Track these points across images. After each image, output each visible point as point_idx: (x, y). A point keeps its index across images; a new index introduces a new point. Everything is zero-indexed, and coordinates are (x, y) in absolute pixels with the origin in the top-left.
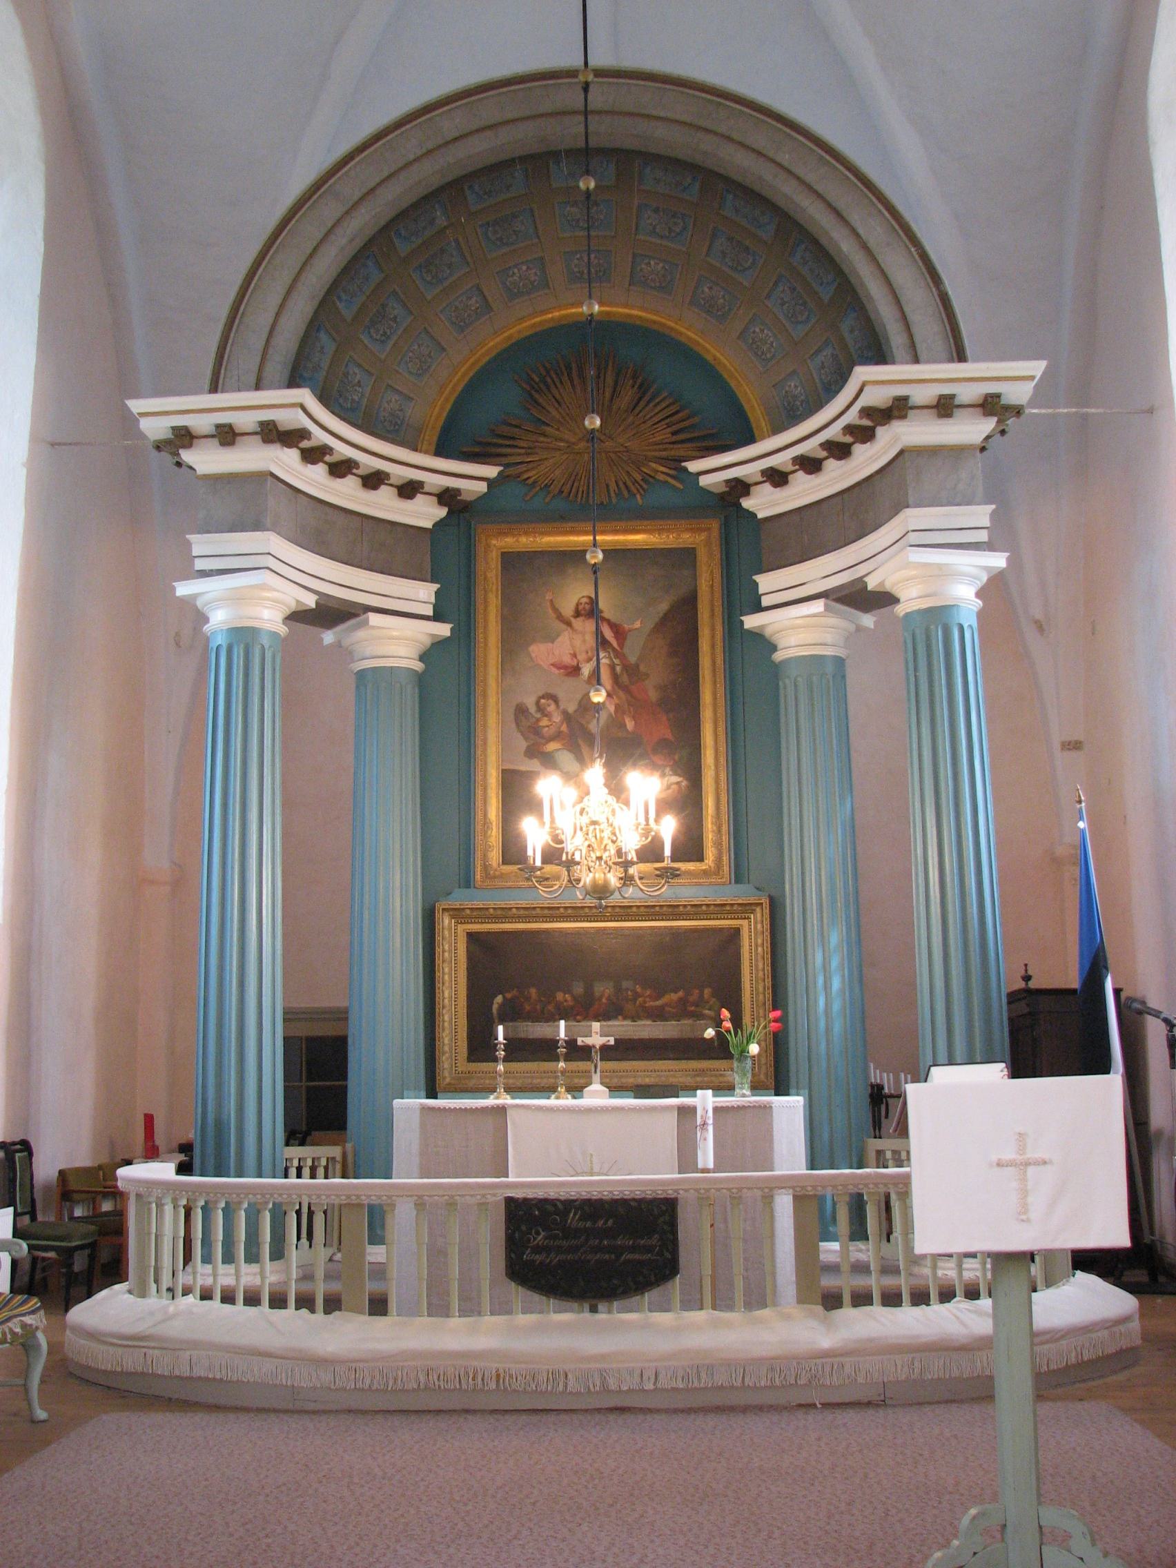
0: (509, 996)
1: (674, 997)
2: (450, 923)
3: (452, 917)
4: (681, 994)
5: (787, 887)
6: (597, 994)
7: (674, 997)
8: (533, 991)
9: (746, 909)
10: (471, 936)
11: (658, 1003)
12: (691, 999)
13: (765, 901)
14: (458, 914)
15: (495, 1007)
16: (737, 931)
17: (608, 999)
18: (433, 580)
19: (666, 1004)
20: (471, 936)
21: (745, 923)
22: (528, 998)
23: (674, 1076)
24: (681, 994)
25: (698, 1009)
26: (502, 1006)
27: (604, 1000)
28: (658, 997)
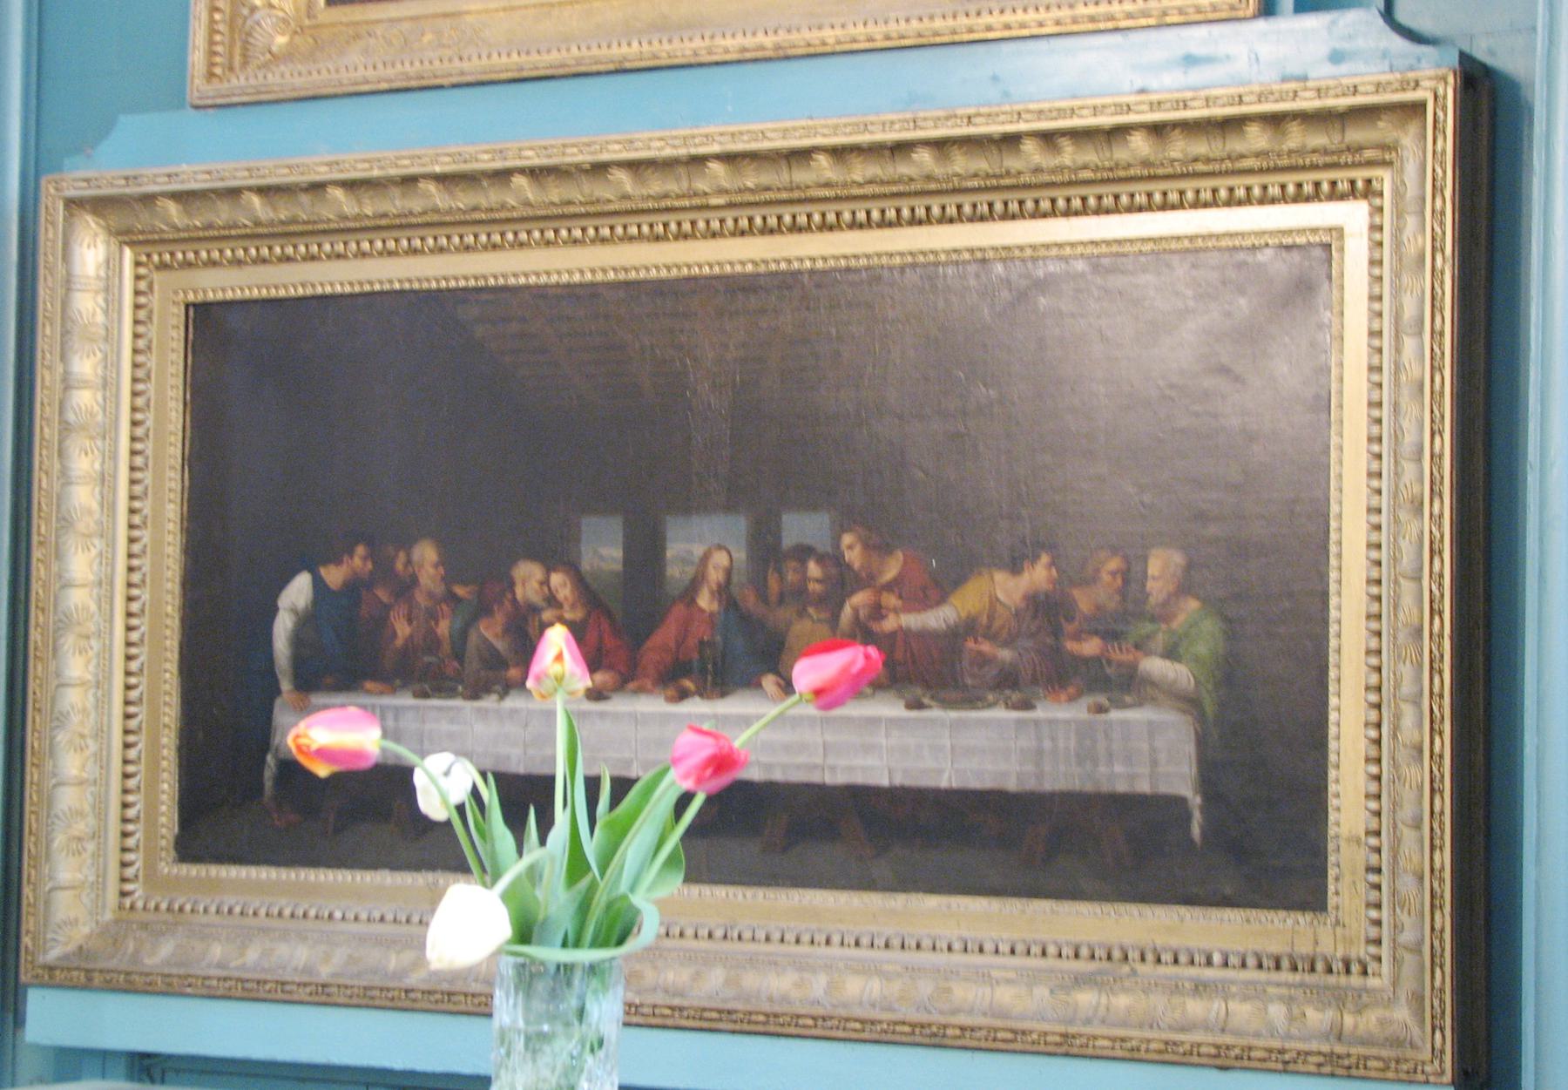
0: (334, 576)
1: (1006, 590)
2: (112, 265)
3: (125, 236)
4: (1038, 575)
5: (191, 336)
6: (676, 572)
7: (1006, 590)
8: (426, 554)
9: (1322, 142)
10: (205, 320)
11: (937, 618)
12: (1084, 601)
13: (1435, 84)
14: (119, 210)
15: (283, 626)
16: (1327, 246)
17: (724, 591)
18: (729, 507)
19: (968, 628)
20: (205, 320)
21: (1352, 216)
22: (406, 587)
23: (984, 977)
24: (1038, 575)
25: (1120, 655)
26: (307, 621)
27: (705, 601)
28: (936, 591)
